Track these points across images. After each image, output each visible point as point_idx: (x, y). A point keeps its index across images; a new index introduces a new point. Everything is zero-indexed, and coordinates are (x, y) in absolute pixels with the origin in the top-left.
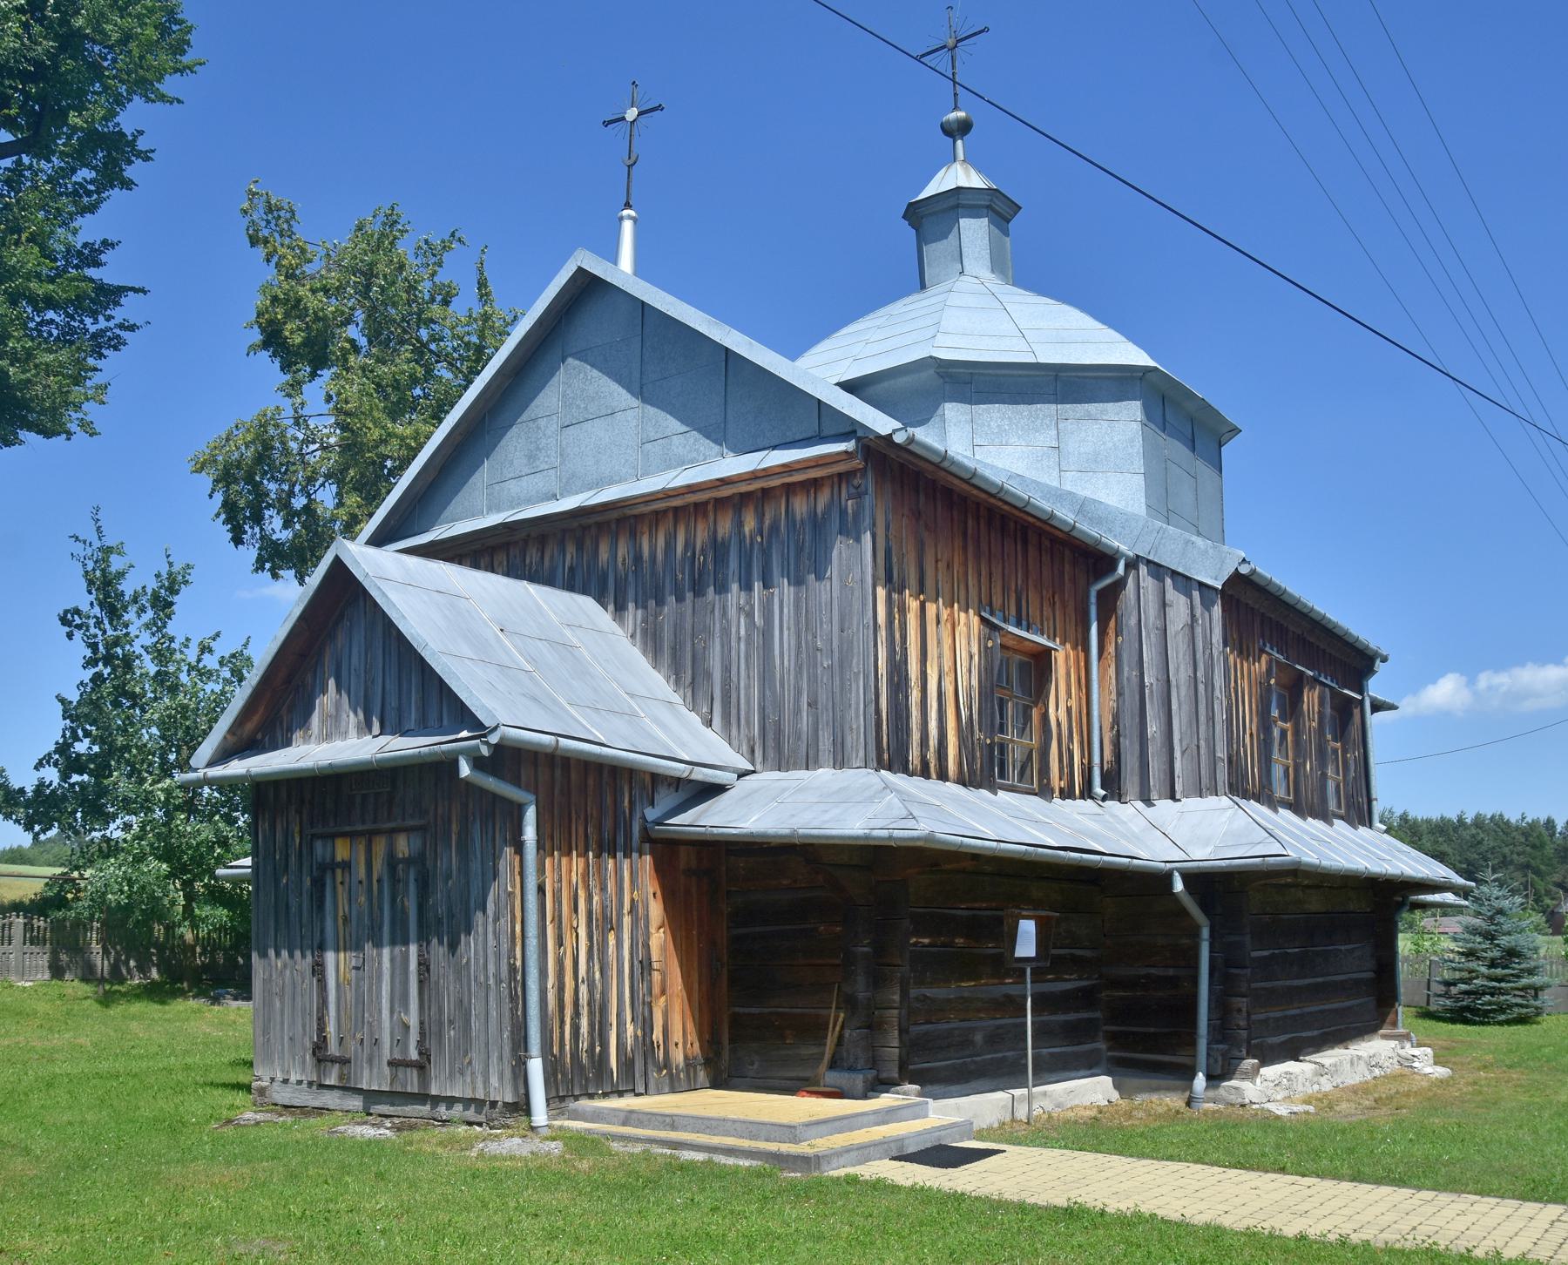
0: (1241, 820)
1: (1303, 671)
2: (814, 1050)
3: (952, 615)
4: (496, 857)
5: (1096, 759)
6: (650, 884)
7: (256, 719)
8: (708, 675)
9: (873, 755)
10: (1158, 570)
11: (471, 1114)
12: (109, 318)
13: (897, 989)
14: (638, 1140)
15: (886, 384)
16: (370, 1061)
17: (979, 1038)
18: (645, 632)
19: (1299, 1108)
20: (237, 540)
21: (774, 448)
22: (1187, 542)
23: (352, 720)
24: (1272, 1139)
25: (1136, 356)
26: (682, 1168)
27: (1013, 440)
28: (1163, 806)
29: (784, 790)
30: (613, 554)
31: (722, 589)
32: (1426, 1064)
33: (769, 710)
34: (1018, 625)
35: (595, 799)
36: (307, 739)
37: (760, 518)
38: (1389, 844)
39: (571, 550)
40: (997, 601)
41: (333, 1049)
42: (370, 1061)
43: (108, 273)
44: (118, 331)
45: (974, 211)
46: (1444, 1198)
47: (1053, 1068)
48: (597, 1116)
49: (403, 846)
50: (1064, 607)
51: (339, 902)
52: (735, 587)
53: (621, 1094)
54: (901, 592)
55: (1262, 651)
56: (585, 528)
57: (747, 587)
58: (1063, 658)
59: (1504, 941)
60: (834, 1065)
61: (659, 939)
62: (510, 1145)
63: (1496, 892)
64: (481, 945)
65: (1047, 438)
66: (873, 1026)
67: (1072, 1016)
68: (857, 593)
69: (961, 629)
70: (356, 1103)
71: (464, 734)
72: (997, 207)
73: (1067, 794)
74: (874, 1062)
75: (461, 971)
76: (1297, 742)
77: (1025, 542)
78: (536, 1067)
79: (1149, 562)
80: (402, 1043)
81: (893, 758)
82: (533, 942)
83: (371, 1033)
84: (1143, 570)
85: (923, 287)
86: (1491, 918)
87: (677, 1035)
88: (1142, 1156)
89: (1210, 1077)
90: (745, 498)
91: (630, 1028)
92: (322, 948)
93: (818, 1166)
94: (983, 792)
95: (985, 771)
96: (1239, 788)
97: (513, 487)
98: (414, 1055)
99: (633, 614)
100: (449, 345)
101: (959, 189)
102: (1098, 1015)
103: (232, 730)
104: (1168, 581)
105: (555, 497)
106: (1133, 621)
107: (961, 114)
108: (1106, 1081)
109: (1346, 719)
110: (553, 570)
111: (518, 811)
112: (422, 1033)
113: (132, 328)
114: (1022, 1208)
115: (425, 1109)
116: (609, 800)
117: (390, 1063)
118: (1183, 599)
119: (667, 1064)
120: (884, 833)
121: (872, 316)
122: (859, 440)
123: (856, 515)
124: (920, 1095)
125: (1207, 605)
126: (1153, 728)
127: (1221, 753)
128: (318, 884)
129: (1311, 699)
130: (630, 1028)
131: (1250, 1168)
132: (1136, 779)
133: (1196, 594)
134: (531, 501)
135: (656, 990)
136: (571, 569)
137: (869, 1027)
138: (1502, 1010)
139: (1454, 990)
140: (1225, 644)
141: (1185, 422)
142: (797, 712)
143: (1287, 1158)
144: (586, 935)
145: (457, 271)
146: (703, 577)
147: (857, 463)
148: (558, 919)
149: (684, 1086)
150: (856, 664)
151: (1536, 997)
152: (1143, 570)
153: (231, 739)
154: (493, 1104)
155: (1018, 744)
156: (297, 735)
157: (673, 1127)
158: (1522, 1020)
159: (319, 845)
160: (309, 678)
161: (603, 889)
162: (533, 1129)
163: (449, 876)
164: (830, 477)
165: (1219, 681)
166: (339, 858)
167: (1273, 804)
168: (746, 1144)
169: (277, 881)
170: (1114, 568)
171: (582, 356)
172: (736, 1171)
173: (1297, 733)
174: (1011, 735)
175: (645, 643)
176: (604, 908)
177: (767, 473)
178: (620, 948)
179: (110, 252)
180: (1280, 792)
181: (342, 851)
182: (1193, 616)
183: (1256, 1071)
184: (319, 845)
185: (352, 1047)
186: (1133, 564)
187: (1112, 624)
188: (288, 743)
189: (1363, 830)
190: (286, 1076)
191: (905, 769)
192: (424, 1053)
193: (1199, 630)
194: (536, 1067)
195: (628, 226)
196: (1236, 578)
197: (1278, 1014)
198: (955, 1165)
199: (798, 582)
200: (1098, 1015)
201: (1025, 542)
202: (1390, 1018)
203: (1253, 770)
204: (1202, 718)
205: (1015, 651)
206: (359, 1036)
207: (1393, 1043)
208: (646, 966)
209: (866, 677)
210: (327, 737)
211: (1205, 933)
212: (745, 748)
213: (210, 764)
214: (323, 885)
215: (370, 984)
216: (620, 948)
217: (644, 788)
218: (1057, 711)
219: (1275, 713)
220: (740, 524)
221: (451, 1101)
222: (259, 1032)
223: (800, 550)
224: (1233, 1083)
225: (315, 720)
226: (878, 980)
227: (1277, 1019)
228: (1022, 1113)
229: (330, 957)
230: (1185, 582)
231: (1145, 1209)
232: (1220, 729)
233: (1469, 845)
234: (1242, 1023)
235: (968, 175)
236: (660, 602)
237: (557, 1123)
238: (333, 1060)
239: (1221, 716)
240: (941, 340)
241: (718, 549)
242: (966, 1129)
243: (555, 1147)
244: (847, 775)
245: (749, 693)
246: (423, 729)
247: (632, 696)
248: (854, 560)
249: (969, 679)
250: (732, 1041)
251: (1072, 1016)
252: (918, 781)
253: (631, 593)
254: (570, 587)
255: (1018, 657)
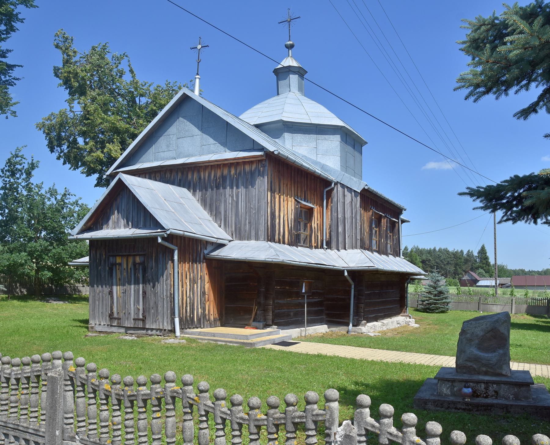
0: (363, 256)
1: (383, 213)
2: (248, 317)
3: (287, 199)
4: (166, 264)
5: (325, 238)
6: (205, 271)
7: (92, 222)
8: (220, 213)
9: (266, 237)
10: (343, 186)
11: (158, 333)
12: (10, 76)
13: (272, 300)
14: (205, 339)
15: (267, 126)
16: (127, 319)
17: (292, 314)
18: (202, 200)
19: (377, 334)
20: (52, 151)
21: (241, 151)
22: (351, 178)
23: (122, 222)
24: (368, 340)
25: (340, 123)
26: (219, 346)
27: (304, 145)
28: (343, 251)
29: (242, 246)
30: (193, 177)
31: (225, 188)
32: (413, 324)
33: (237, 223)
34: (305, 201)
35: (192, 248)
36: (108, 228)
37: (236, 170)
38: (404, 262)
39: (180, 175)
40: (299, 194)
41: (115, 315)
42: (127, 319)
43: (9, 60)
44: (13, 80)
45: (295, 73)
46: (408, 353)
47: (311, 322)
48: (192, 333)
49: (138, 260)
50: (317, 194)
51: (117, 274)
52: (228, 187)
53: (197, 328)
54: (274, 193)
55: (371, 209)
56: (184, 168)
57: (232, 188)
58: (316, 209)
59: (439, 289)
60: (254, 321)
61: (207, 286)
62: (171, 341)
63: (437, 275)
64: (162, 287)
65: (314, 144)
66: (265, 310)
67: (316, 309)
68: (263, 193)
69: (290, 203)
70: (123, 330)
71: (159, 230)
72: (300, 72)
73: (316, 247)
74: (265, 320)
75: (155, 294)
76: (379, 234)
77: (307, 177)
78: (177, 320)
79: (341, 183)
80: (138, 314)
81: (271, 238)
82: (176, 287)
83: (128, 311)
84: (339, 185)
85: (278, 94)
86: (435, 282)
87: (212, 312)
88: (335, 344)
89: (353, 326)
90: (232, 164)
91: (200, 310)
92: (112, 285)
93: (254, 346)
94: (294, 247)
95: (295, 241)
96: (363, 247)
97: (162, 155)
98: (141, 317)
99: (199, 194)
100: (123, 92)
101: (290, 66)
102: (324, 308)
103: (84, 225)
104: (346, 189)
105: (175, 158)
106: (336, 200)
107: (291, 42)
108: (326, 326)
109: (394, 227)
110: (174, 180)
111: (172, 252)
112: (144, 311)
113: (17, 79)
114: (307, 355)
115: (144, 332)
116: (195, 248)
117: (133, 319)
118: (349, 194)
119: (209, 320)
120: (271, 260)
121: (263, 103)
122: (265, 152)
123: (263, 172)
124: (277, 328)
125: (356, 196)
126: (340, 229)
127: (359, 238)
128: (111, 270)
129: (384, 221)
130: (200, 310)
131: (362, 347)
132: (335, 244)
133: (353, 193)
134: (168, 159)
135: (207, 300)
136: (180, 180)
137: (264, 310)
138: (437, 309)
139: (424, 303)
140: (361, 207)
141: (352, 141)
142: (245, 225)
143: (372, 344)
144: (187, 283)
145: (124, 66)
146: (220, 184)
147: (264, 158)
148: (182, 281)
149: (213, 326)
150: (262, 213)
151: (447, 305)
152: (339, 185)
153: (84, 227)
154: (165, 330)
155: (303, 234)
156: (105, 226)
157: (214, 336)
158: (443, 312)
159: (111, 258)
160: (108, 211)
161: (193, 272)
162: (176, 337)
163: (152, 268)
164: (256, 161)
165: (358, 218)
166: (117, 262)
167: (372, 251)
168: (235, 340)
169: (97, 269)
170: (331, 185)
171: (184, 117)
172: (234, 347)
173: (380, 231)
174: (302, 231)
175: (202, 203)
176: (193, 277)
177: (239, 158)
178: (197, 288)
179: (10, 53)
180: (374, 248)
181: (119, 260)
182: (352, 199)
183: (366, 324)
184: (111, 258)
185: (121, 315)
186: (336, 184)
187: (330, 200)
188: (102, 229)
189: (397, 258)
190: (99, 324)
191: (274, 242)
192: (144, 317)
193: (353, 203)
194: (177, 320)
195: (197, 80)
196: (364, 189)
197: (372, 309)
198: (288, 346)
199: (246, 187)
200: (324, 308)
201: (307, 177)
202: (404, 310)
203: (367, 242)
204: (354, 228)
205: (304, 208)
206: (124, 312)
207: (404, 317)
208: (204, 293)
209: (265, 216)
210: (115, 228)
211: (353, 287)
212: (230, 234)
213: (78, 234)
214: (113, 270)
215: (127, 296)
216: (197, 288)
217: (204, 244)
218: (314, 225)
219: (374, 226)
220: (230, 172)
221: (152, 330)
222: (91, 311)
223: (247, 180)
224: (359, 327)
225: (110, 222)
226: (266, 298)
227: (372, 310)
228: (303, 334)
229: (115, 288)
230: (350, 190)
231: (336, 355)
232: (358, 231)
233: (430, 261)
234: (362, 311)
235: (293, 62)
236: (206, 190)
237: (182, 335)
238: (115, 319)
239: (359, 228)
240: (284, 114)
241: (224, 178)
242: (290, 337)
243: (184, 341)
244: (259, 242)
245: (232, 219)
246: (145, 227)
247: (200, 218)
248: (262, 183)
249: (291, 216)
250: (225, 314)
251: (316, 309)
252: (277, 244)
253: (198, 188)
254: (179, 185)
255: (304, 210)
